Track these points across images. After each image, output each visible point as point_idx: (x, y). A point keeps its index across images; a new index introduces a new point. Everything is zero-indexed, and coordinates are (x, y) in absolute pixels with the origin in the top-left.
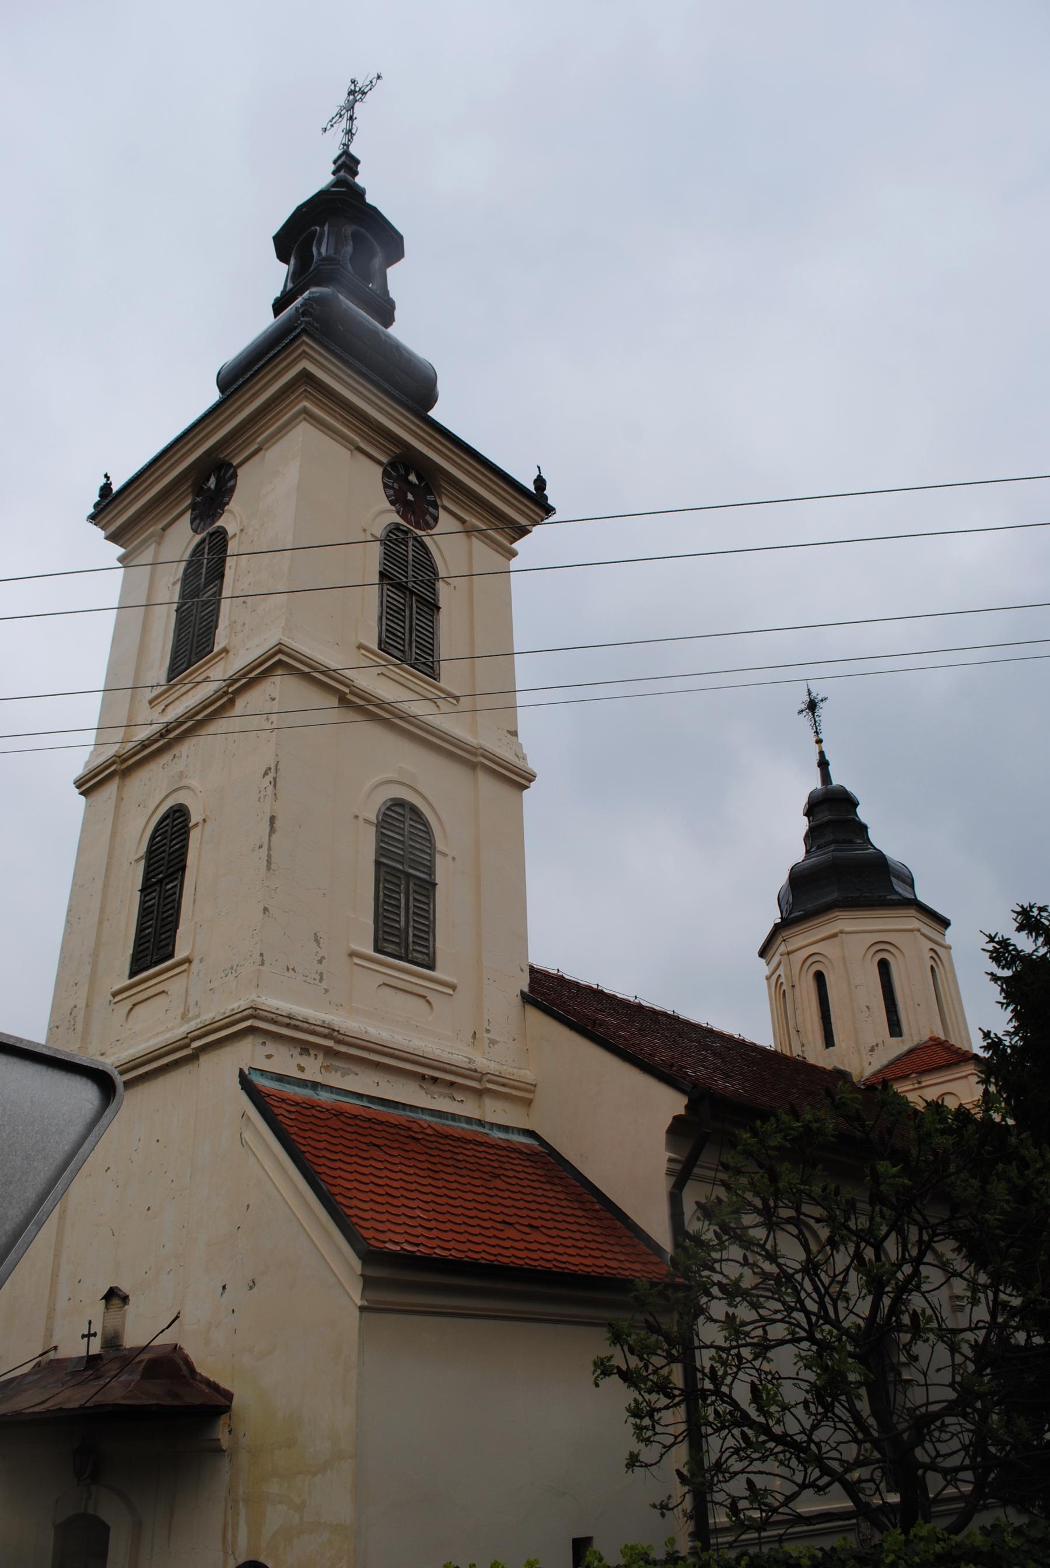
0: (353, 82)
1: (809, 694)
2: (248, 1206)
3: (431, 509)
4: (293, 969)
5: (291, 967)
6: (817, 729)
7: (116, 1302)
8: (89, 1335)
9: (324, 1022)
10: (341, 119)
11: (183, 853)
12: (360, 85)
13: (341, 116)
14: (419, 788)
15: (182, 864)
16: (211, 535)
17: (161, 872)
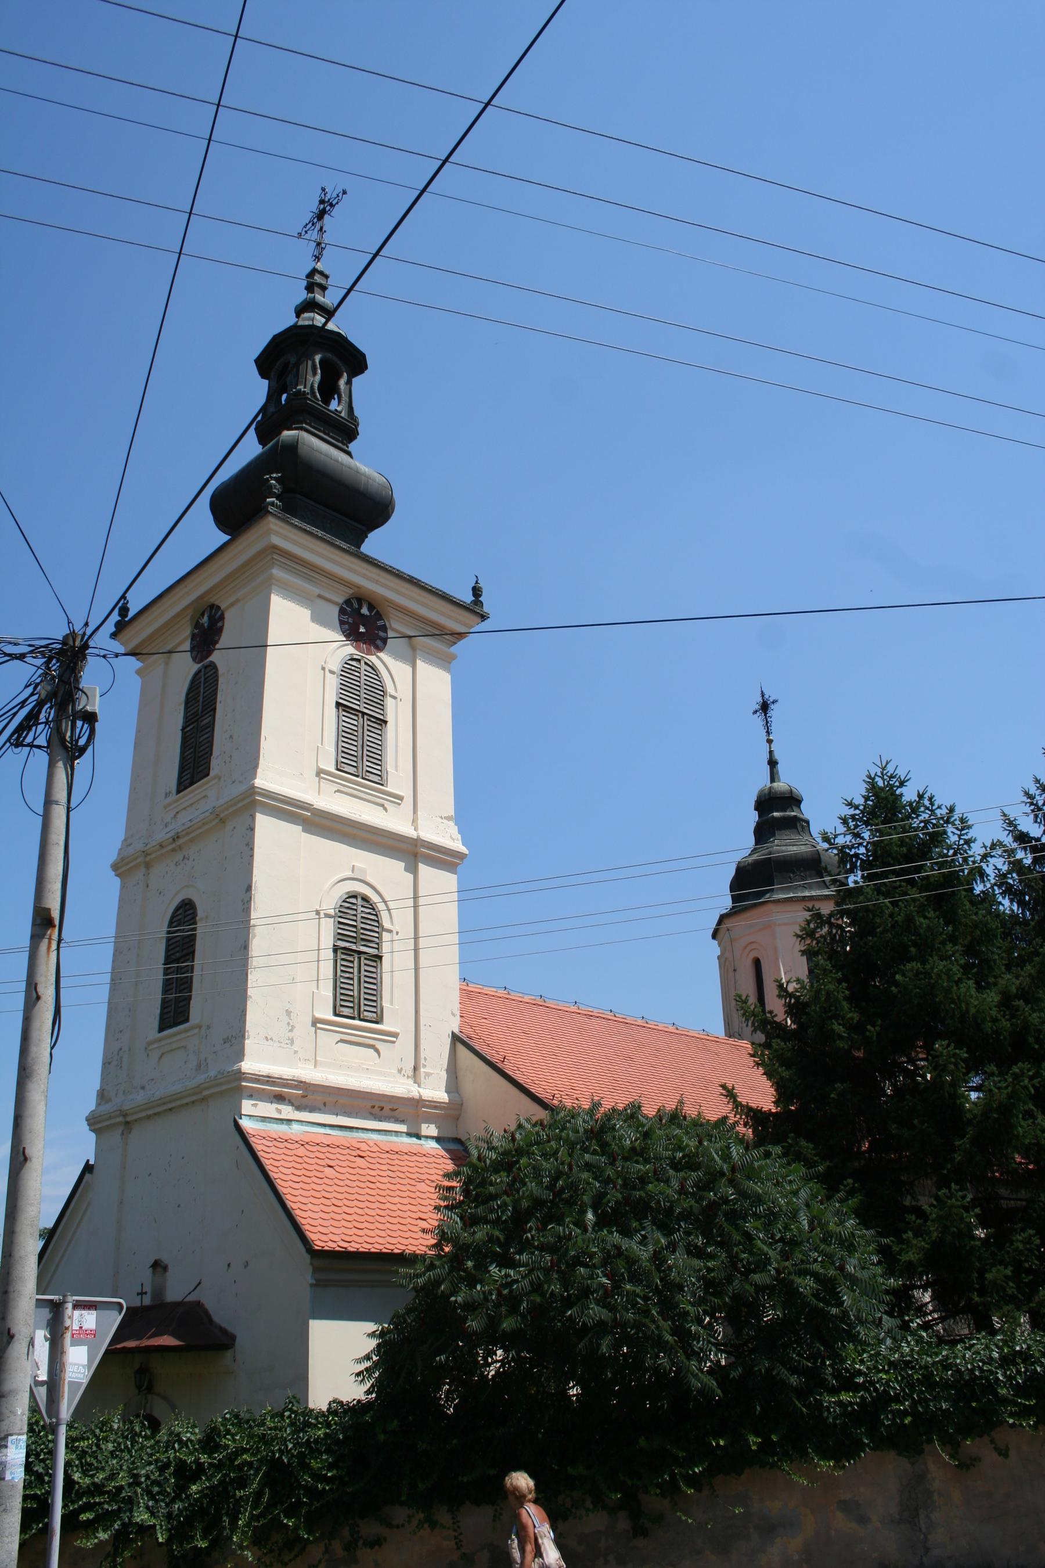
0: (323, 189)
1: (763, 695)
2: (243, 1211)
3: (381, 634)
4: (272, 1039)
5: (269, 1038)
6: (768, 728)
7: (159, 1269)
8: (142, 1294)
9: (294, 1076)
10: (313, 227)
11: (192, 945)
12: (328, 196)
13: (313, 224)
14: (369, 879)
15: (191, 950)
16: (206, 667)
17: (178, 952)
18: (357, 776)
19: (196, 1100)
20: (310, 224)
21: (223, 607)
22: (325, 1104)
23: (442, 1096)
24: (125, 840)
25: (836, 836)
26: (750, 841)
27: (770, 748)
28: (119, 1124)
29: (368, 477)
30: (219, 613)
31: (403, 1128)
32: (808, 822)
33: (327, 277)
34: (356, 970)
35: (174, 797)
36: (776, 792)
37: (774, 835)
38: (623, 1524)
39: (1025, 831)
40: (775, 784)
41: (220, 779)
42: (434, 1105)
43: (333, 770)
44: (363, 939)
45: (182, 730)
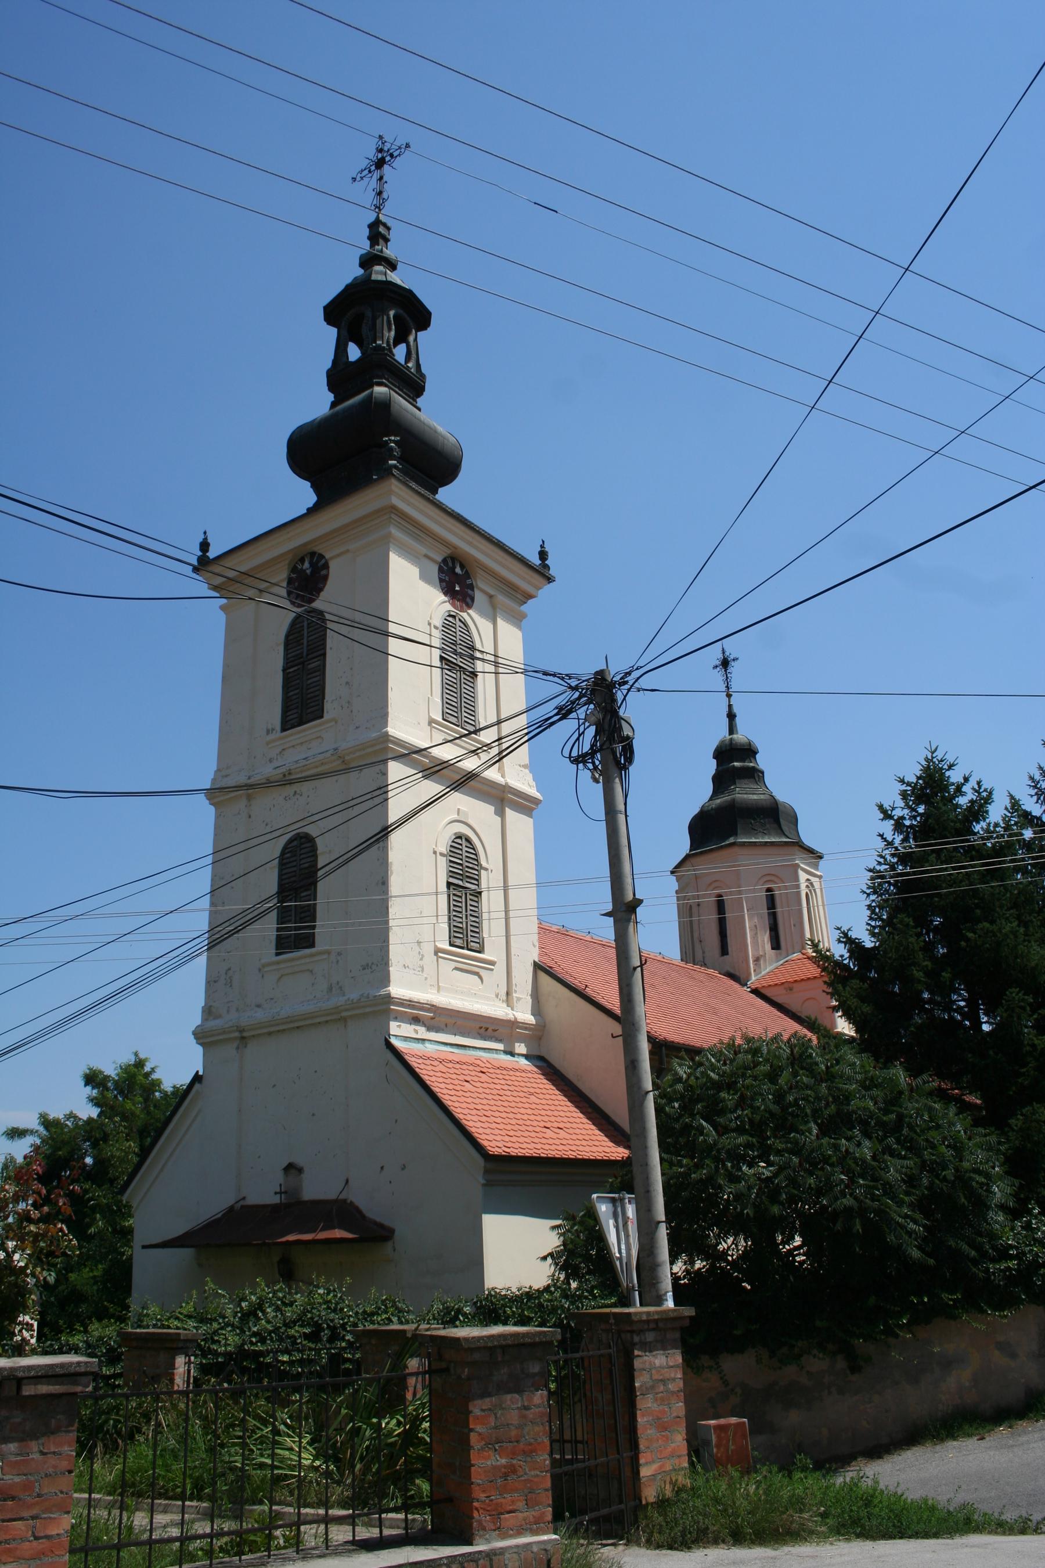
1: (724, 653)
3: (470, 592)
10: (370, 175)
13: (370, 172)
14: (470, 822)
18: (458, 726)
19: (331, 1020)
20: (366, 172)
21: (327, 556)
22: (446, 1025)
23: (530, 1019)
24: (218, 770)
25: (893, 809)
26: (708, 789)
27: (729, 702)
28: (235, 1038)
29: (444, 438)
30: (323, 561)
31: (500, 1046)
32: (763, 773)
33: (389, 229)
34: (464, 904)
35: (278, 734)
36: (736, 743)
37: (735, 783)
38: (841, 1364)
39: (1029, 810)
40: (735, 736)
41: (336, 722)
42: (525, 1026)
43: (440, 720)
44: (467, 877)
45: (284, 670)
